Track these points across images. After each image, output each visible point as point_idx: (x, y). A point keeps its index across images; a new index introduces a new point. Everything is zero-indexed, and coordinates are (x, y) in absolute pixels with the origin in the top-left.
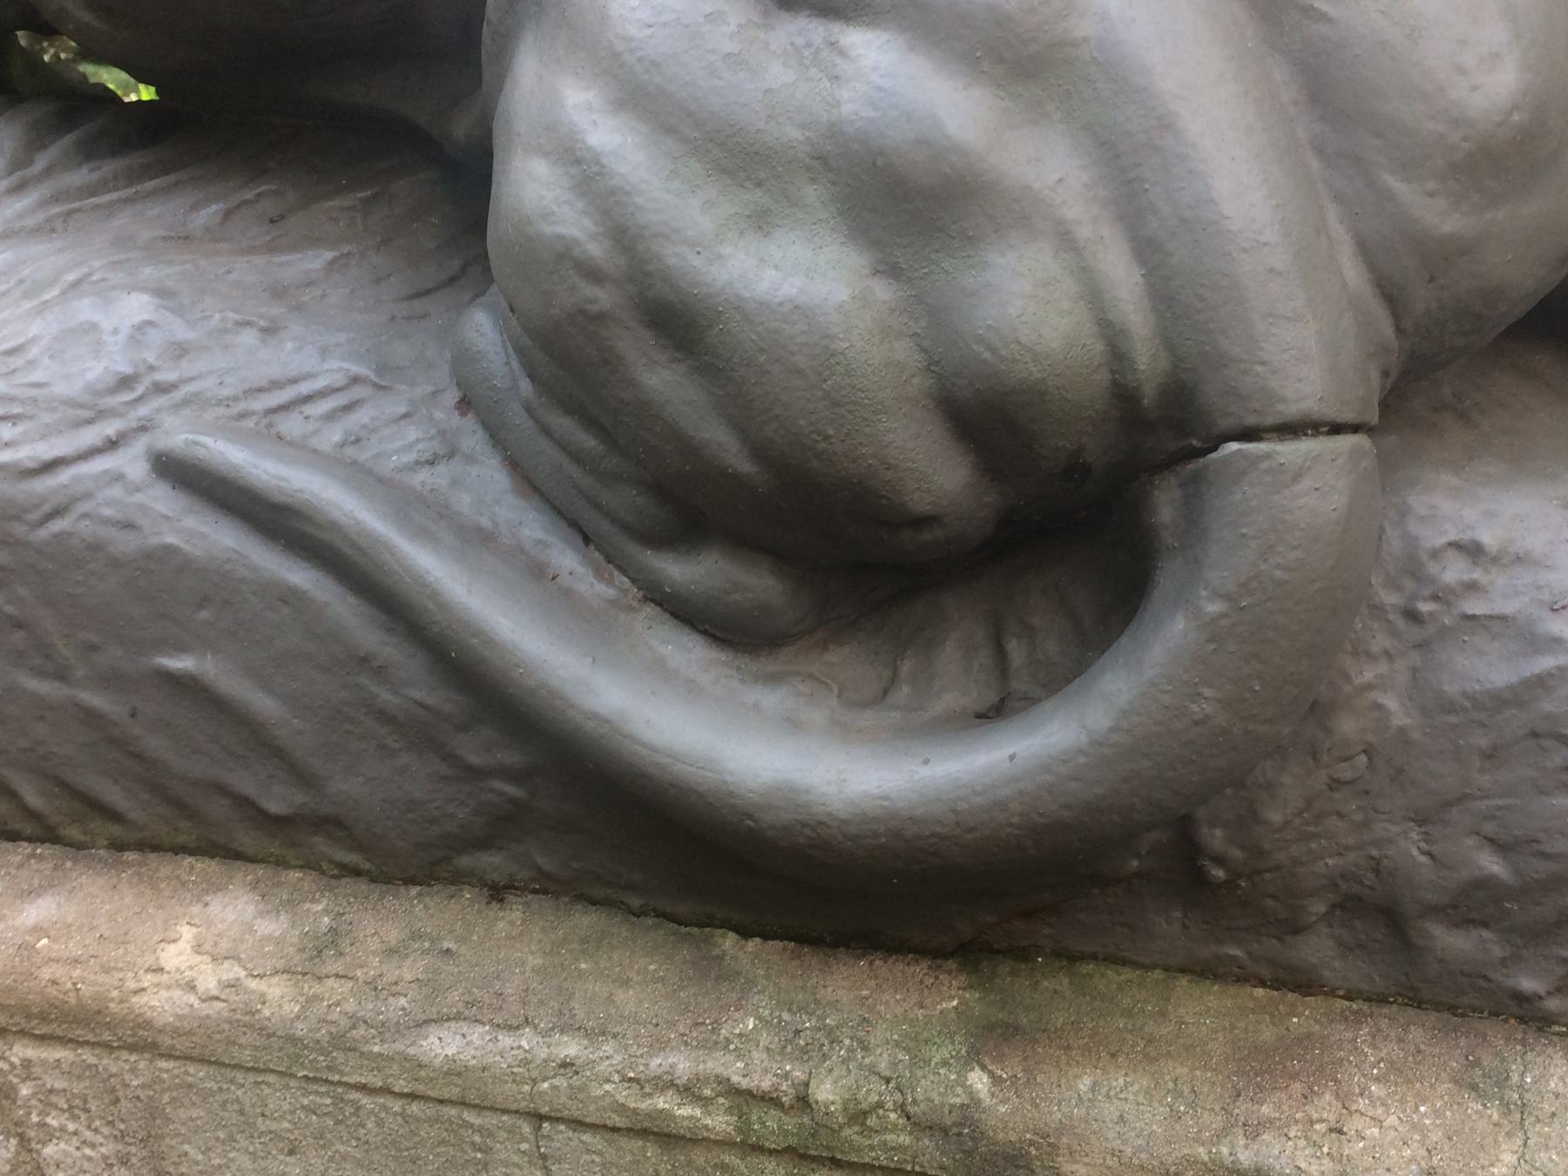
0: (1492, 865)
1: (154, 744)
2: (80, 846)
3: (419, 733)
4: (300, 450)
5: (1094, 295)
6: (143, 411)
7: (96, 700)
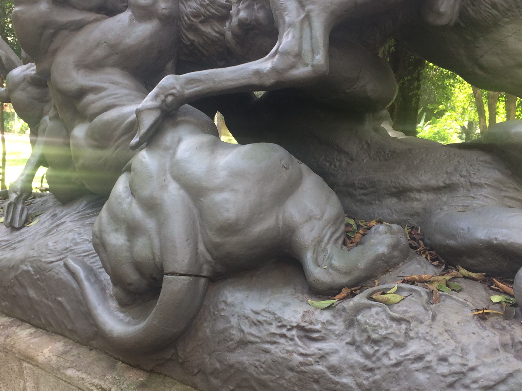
0: (218, 365)
2: (48, 331)
5: (152, 248)
6: (67, 254)
7: (51, 304)
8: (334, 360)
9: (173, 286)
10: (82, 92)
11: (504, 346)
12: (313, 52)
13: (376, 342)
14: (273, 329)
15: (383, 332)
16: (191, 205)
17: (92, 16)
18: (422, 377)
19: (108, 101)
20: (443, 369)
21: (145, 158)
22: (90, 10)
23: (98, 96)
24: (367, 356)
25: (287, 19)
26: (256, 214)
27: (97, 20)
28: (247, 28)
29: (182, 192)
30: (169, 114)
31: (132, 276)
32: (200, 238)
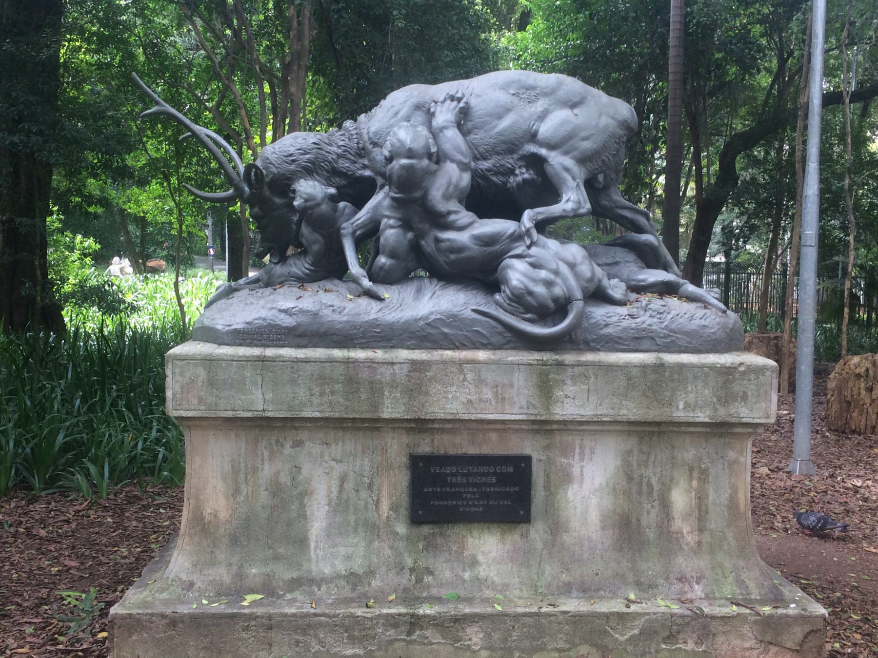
3: (500, 334)
18: (681, 320)
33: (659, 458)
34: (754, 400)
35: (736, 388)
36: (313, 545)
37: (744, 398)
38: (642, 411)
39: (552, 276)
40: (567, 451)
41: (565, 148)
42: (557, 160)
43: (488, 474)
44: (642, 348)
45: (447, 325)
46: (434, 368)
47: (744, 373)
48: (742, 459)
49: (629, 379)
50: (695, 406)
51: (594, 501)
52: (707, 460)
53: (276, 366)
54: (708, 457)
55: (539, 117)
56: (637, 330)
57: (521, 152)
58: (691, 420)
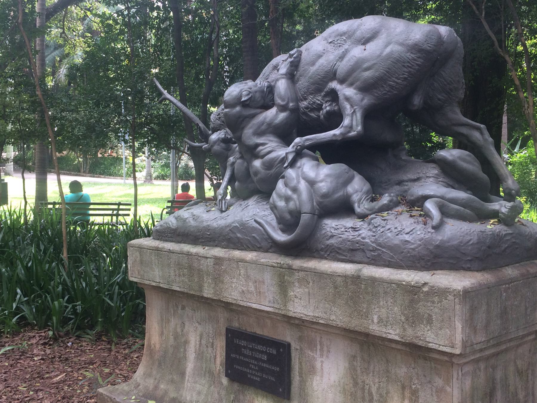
1: (252, 242)
4: (262, 219)
8: (363, 235)
9: (305, 218)
10: (257, 145)
11: (415, 222)
12: (357, 126)
13: (376, 227)
14: (343, 230)
15: (379, 224)
16: (310, 188)
17: (258, 111)
18: (389, 235)
19: (269, 149)
20: (396, 230)
21: (291, 173)
22: (258, 108)
23: (264, 147)
24: (374, 232)
25: (346, 112)
26: (335, 190)
27: (261, 112)
28: (329, 114)
29: (307, 183)
30: (299, 154)
31: (288, 217)
32: (314, 200)
33: (377, 369)
34: (439, 325)
35: (422, 308)
36: (187, 378)
37: (430, 321)
38: (346, 319)
39: (289, 193)
40: (312, 345)
41: (350, 80)
42: (347, 91)
43: (262, 352)
44: (356, 259)
45: (240, 231)
46: (225, 263)
47: (427, 294)
48: (448, 389)
49: (336, 288)
50: (387, 322)
51: (330, 396)
52: (416, 382)
53: (162, 254)
54: (418, 379)
55: (340, 58)
56: (352, 242)
57: (325, 90)
58: (384, 336)
